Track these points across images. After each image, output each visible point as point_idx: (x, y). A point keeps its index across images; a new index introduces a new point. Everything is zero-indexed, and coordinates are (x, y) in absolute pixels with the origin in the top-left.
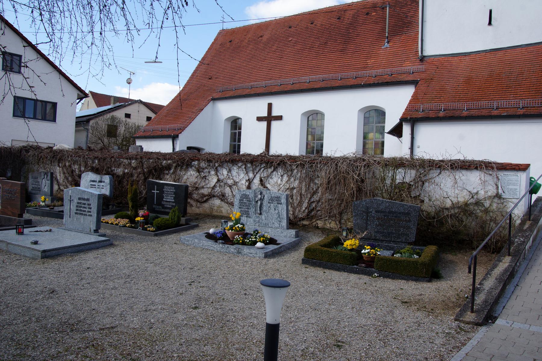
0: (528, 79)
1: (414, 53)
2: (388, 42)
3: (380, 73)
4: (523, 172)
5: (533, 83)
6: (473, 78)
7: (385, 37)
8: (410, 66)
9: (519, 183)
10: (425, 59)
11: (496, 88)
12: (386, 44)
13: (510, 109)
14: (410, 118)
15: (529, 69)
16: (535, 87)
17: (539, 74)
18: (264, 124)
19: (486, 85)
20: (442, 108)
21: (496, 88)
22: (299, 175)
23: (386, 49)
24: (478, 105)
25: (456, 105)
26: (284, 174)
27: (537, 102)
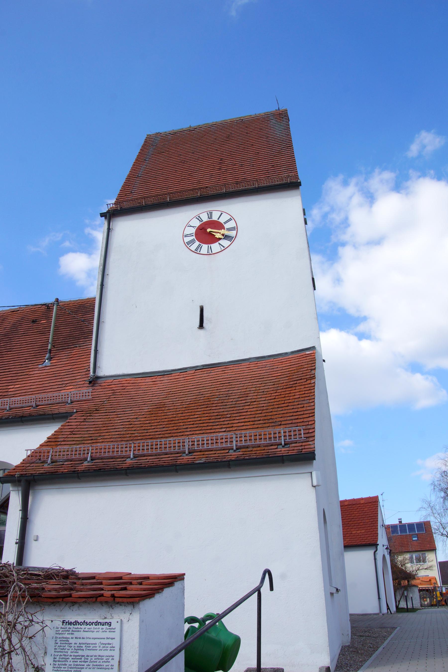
0: (255, 403)
2: (50, 359)
4: (129, 609)
5: (262, 408)
6: (166, 406)
9: (117, 658)
10: (99, 381)
11: (199, 419)
13: (215, 452)
15: (258, 389)
16: (264, 415)
17: (273, 395)
19: (184, 415)
21: (199, 419)
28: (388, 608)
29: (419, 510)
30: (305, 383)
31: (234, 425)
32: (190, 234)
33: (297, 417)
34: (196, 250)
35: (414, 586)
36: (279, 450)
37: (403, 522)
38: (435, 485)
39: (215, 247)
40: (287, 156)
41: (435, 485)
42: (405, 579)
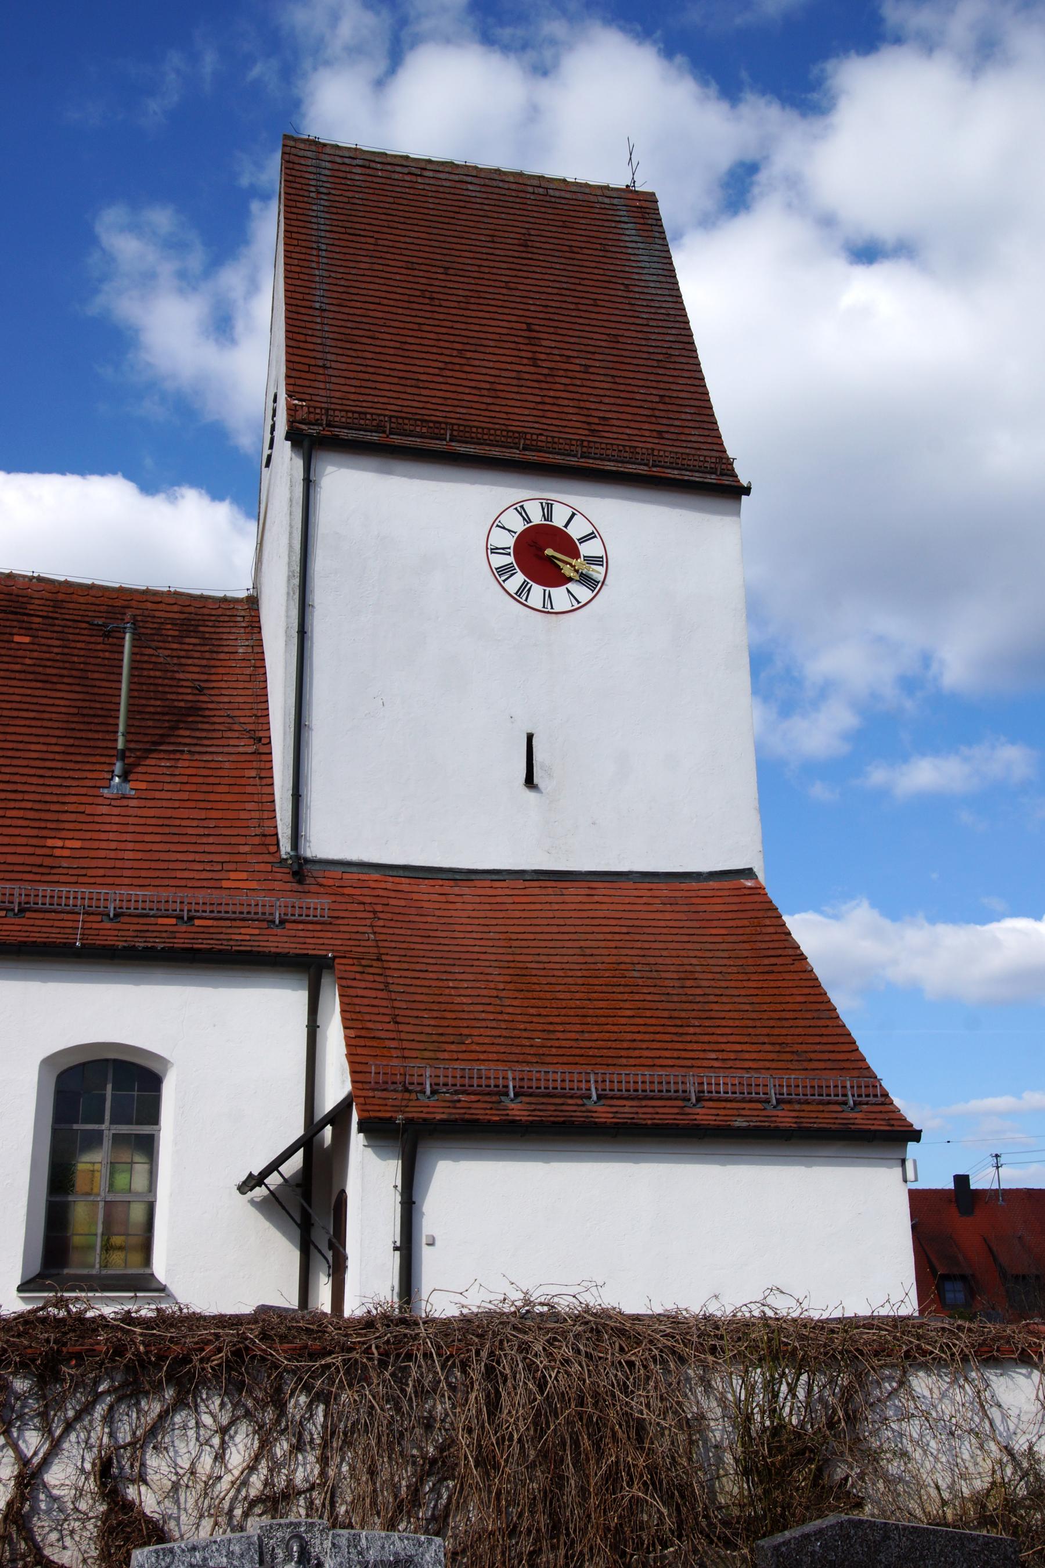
3: (140, 905)
7: (114, 752)
12: (117, 779)
14: (406, 1119)
20: (507, 1087)
22: (320, 1418)
23: (125, 802)
24: (669, 1083)
25: (554, 1076)
26: (232, 1423)
27: (808, 1085)
32: (503, 549)
34: (519, 592)
39: (559, 595)
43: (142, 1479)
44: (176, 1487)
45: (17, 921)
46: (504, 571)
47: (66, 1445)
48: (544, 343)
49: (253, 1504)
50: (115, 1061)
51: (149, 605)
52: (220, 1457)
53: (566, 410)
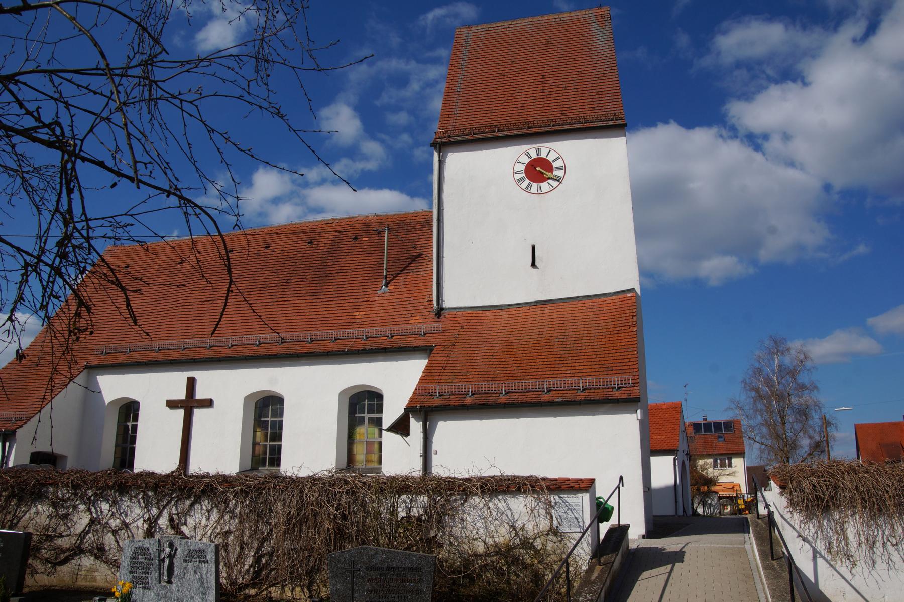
1: (427, 303)
2: (387, 285)
8: (421, 324)
18: (181, 413)
23: (384, 295)
25: (485, 386)
28: (684, 511)
29: (726, 410)
30: (629, 330)
31: (577, 368)
33: (624, 364)
34: (527, 188)
35: (716, 493)
36: (614, 393)
37: (708, 420)
38: (746, 383)
39: (545, 186)
40: (611, 80)
41: (746, 383)
42: (704, 484)
43: (185, 524)
44: (195, 526)
45: (257, 348)
46: (521, 180)
47: (164, 513)
48: (548, 82)
49: (219, 534)
50: (368, 391)
51: (414, 218)
52: (208, 519)
53: (553, 108)
